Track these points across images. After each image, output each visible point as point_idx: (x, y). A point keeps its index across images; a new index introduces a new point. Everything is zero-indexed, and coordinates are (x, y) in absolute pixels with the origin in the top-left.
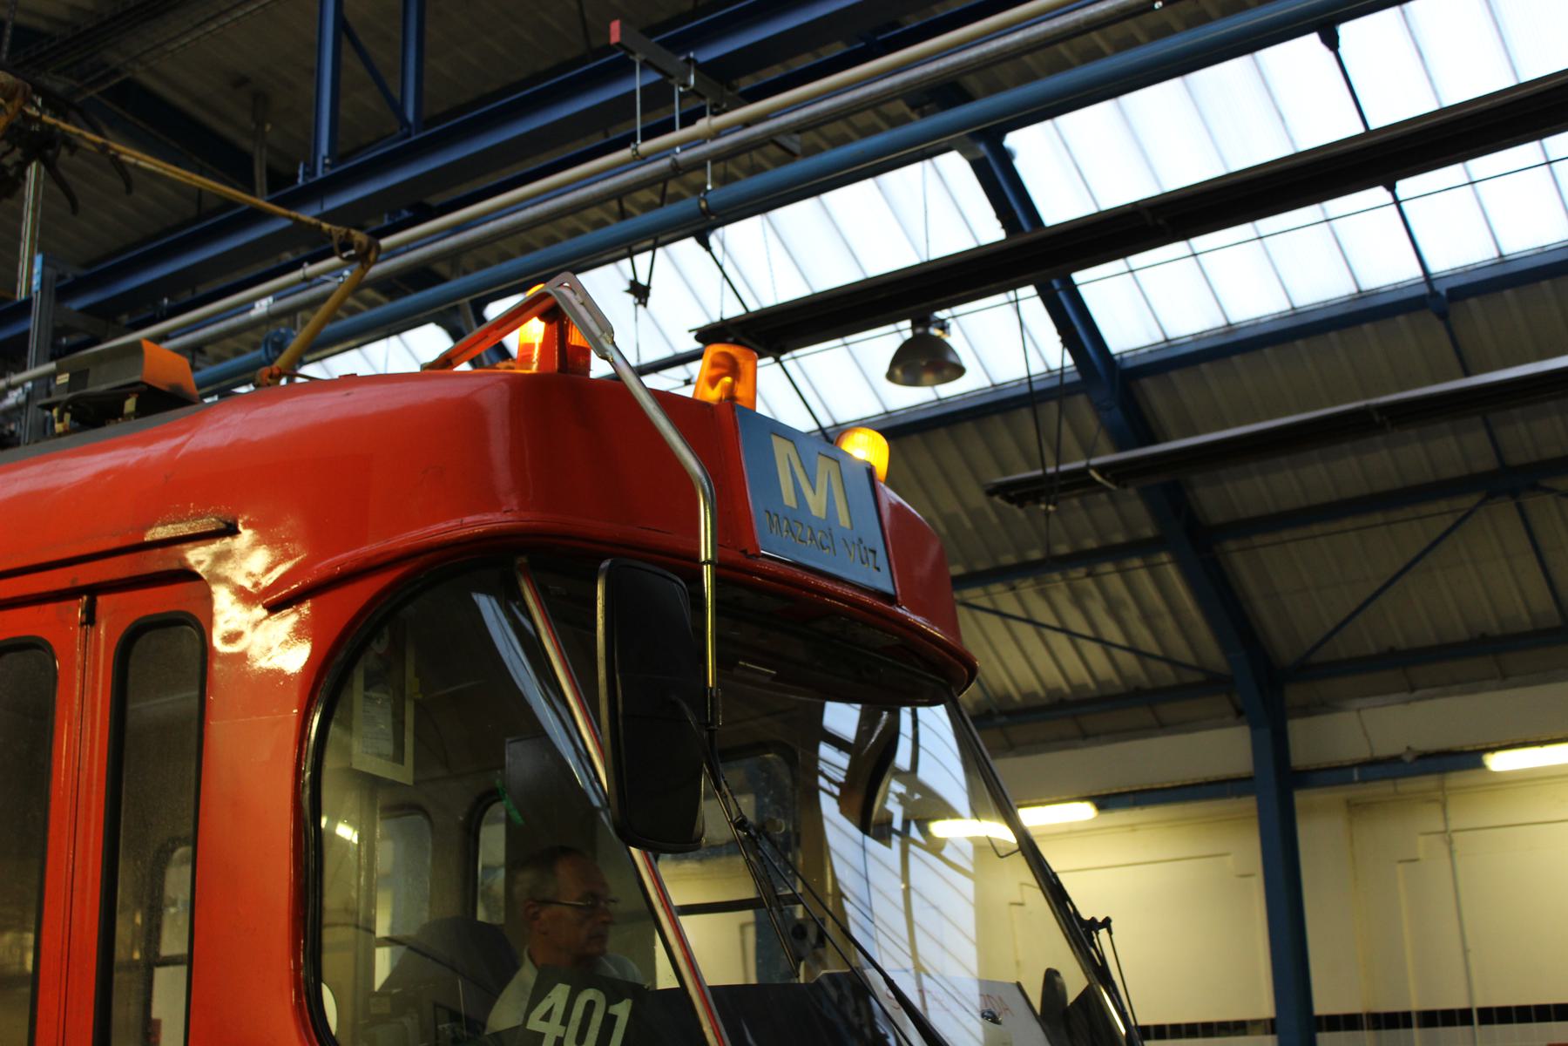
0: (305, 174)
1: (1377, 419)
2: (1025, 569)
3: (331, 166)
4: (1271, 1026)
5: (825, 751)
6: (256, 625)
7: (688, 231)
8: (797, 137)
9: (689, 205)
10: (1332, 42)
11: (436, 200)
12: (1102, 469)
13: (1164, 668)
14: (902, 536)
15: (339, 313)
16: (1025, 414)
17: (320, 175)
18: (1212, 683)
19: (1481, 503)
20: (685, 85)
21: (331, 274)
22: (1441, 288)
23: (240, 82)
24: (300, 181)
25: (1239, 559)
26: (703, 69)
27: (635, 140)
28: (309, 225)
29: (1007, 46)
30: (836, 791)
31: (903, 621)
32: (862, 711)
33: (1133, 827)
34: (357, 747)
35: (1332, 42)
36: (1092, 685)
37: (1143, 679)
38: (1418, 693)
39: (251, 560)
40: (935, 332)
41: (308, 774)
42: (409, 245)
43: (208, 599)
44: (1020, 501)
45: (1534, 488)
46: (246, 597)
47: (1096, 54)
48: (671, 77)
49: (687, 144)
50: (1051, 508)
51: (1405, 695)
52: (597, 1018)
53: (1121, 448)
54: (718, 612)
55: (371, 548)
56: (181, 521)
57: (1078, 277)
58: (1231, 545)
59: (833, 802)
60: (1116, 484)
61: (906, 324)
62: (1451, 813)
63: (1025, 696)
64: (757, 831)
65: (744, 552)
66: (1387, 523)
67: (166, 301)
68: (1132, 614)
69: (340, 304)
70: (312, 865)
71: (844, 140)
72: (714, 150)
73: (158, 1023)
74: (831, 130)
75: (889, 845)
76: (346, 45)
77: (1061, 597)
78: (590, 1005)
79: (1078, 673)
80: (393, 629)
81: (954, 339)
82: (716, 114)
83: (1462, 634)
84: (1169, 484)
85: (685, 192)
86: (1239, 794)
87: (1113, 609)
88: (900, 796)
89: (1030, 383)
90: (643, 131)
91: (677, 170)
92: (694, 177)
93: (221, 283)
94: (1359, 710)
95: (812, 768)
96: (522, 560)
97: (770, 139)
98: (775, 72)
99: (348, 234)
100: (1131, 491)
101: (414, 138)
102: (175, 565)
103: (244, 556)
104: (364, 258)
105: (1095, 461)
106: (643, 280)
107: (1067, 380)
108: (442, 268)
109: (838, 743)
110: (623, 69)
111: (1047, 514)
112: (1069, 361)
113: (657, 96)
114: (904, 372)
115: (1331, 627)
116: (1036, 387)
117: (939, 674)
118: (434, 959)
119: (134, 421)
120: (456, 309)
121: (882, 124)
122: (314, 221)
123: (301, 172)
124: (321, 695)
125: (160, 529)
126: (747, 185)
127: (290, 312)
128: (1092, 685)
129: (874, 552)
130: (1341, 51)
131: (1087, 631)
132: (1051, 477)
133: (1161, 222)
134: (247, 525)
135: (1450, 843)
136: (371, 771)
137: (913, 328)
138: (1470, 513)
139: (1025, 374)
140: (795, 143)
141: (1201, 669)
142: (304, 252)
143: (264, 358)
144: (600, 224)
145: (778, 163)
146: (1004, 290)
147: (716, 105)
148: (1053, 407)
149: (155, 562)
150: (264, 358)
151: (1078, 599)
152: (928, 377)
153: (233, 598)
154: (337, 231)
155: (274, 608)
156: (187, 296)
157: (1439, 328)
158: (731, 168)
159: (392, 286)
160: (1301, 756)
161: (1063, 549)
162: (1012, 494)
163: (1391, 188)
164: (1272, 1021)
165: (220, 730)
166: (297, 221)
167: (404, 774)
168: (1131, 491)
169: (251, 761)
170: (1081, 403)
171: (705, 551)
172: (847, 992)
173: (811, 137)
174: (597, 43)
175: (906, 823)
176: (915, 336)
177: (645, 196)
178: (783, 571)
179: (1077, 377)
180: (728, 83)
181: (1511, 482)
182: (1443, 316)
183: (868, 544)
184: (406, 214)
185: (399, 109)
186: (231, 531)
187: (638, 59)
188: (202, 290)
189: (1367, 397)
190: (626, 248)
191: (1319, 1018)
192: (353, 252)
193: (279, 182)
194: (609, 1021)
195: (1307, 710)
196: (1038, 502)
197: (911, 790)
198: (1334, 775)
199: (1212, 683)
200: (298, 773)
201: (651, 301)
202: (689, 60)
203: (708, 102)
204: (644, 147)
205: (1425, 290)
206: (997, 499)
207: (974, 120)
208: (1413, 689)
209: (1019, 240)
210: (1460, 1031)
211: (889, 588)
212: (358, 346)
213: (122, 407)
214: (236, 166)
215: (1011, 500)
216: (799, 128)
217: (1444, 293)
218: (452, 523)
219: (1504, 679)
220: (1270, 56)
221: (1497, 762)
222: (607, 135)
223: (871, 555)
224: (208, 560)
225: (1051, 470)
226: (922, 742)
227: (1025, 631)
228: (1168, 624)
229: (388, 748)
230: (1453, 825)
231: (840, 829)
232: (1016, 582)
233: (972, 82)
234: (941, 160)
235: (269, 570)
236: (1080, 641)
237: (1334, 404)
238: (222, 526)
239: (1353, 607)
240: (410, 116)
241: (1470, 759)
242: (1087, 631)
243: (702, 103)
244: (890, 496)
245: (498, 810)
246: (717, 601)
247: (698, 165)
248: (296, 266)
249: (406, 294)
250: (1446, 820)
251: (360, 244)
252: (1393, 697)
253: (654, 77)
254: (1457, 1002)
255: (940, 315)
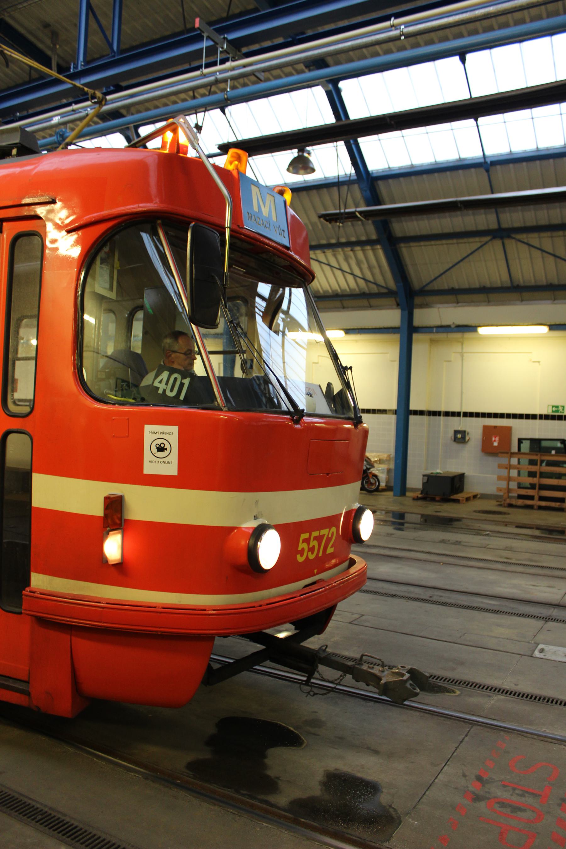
0: (74, 68)
1: (459, 205)
2: (329, 246)
3: (84, 66)
4: (395, 412)
5: (258, 300)
6: (63, 237)
7: (217, 106)
8: (263, 74)
9: (219, 96)
10: (463, 60)
11: (124, 84)
12: (360, 213)
13: (374, 286)
14: (294, 227)
15: (91, 123)
16: (335, 189)
17: (79, 69)
18: (390, 293)
19: (491, 240)
20: (222, 48)
21: (87, 108)
22: (488, 161)
23: (46, 26)
24: (72, 70)
25: (405, 250)
26: (230, 42)
27: (202, 68)
28: (79, 88)
29: (344, 47)
30: (261, 314)
31: (291, 257)
32: (272, 288)
33: (357, 341)
34: (97, 286)
35: (463, 60)
36: (348, 290)
37: (367, 290)
38: (460, 304)
39: (61, 213)
40: (306, 155)
41: (80, 292)
42: (116, 100)
43: (45, 226)
44: (330, 221)
45: (509, 237)
46: (59, 227)
47: (377, 54)
48: (217, 44)
49: (221, 72)
50: (341, 225)
51: (455, 305)
52: (178, 383)
53: (368, 205)
54: (230, 248)
55: (105, 213)
56: (35, 197)
57: (360, 140)
58: (402, 245)
59: (260, 318)
60: (365, 218)
61: (296, 151)
62: (464, 346)
63: (324, 292)
64: (237, 324)
65: (238, 226)
66: (458, 243)
67: (18, 114)
68: (365, 266)
69: (91, 120)
70: (80, 325)
71: (279, 77)
72: (232, 75)
73: (17, 380)
74: (275, 72)
75: (278, 335)
76: (91, 15)
77: (341, 257)
78: (176, 379)
79: (344, 285)
80: (113, 242)
81: (312, 158)
82: (233, 61)
83: (477, 286)
84: (384, 220)
85: (217, 91)
86: (395, 333)
87: (359, 263)
88: (283, 319)
89: (338, 178)
90: (205, 64)
91: (217, 82)
92: (222, 86)
93: (38, 109)
94: (439, 308)
95: (253, 305)
96: (159, 222)
97: (253, 73)
98: (256, 47)
99: (94, 93)
100: (370, 222)
101: (116, 58)
102: (33, 213)
103: (58, 212)
104: (100, 103)
105: (359, 209)
106: (200, 124)
107: (352, 178)
108: (123, 112)
109: (263, 298)
110: (199, 38)
111: (339, 227)
112: (353, 171)
113: (211, 51)
114: (293, 168)
115: (433, 278)
116: (340, 180)
117: (302, 277)
118: (118, 362)
119: (16, 158)
120: (128, 128)
121: (294, 72)
122: (81, 86)
123: (72, 67)
124: (85, 264)
125: (27, 199)
126: (242, 91)
127: (65, 124)
128: (348, 290)
129: (284, 231)
130: (466, 65)
131: (348, 271)
132: (342, 214)
133: (393, 122)
134: (60, 200)
135: (462, 356)
136: (102, 294)
137: (298, 152)
138: (486, 243)
139: (337, 175)
140: (262, 76)
141: (387, 288)
142: (71, 100)
143: (56, 140)
144: (184, 100)
145: (254, 83)
146: (333, 142)
147: (233, 57)
148: (345, 188)
149: (25, 212)
150: (56, 140)
151: (347, 259)
152: (302, 171)
153: (53, 227)
154: (90, 91)
155: (69, 232)
156: (25, 113)
157: (486, 174)
158: (236, 84)
159: (104, 117)
160: (417, 322)
161: (343, 240)
162: (327, 218)
163: (476, 120)
164: (396, 411)
165: (48, 275)
166: (75, 86)
167: (112, 295)
168: (370, 222)
169: (59, 287)
170: (356, 187)
171: (227, 223)
172: (262, 382)
173: (267, 75)
174: (189, 26)
175: (284, 328)
176: (299, 156)
177: (202, 91)
178: (252, 235)
179: (355, 178)
180: (239, 48)
181: (501, 234)
182: (487, 171)
183: (282, 228)
184: (112, 88)
185: (111, 45)
186: (54, 202)
187: (205, 35)
188: (31, 111)
189: (457, 197)
190: (195, 110)
191: (411, 411)
192: (96, 100)
193: (61, 70)
194: (182, 385)
195: (421, 306)
196: (336, 222)
197: (286, 318)
198: (427, 329)
199: (390, 293)
200: (76, 292)
201: (202, 131)
202: (224, 38)
203: (230, 56)
204: (206, 71)
205: (482, 160)
206: (322, 219)
207: (328, 74)
208: (458, 303)
209: (340, 123)
210: (456, 419)
211: (288, 245)
212: (90, 139)
213: (11, 152)
214: (46, 61)
215: (327, 220)
216: (264, 70)
217: (489, 162)
218: (135, 206)
219: (489, 302)
220: (440, 63)
221: (482, 331)
222: (190, 65)
223: (282, 232)
224: (45, 212)
225: (342, 211)
226: (292, 300)
227: (327, 268)
228: (377, 271)
229: (107, 286)
230: (464, 350)
231: (263, 328)
232: (326, 250)
233: (329, 60)
234: (314, 89)
235: (67, 217)
236: (346, 274)
237: (557, 185)
238: (51, 200)
239: (442, 272)
240: (115, 48)
241: (472, 328)
242: (348, 271)
243: (228, 56)
244: (291, 211)
245: (140, 315)
246: (230, 244)
247: (225, 81)
248: (69, 105)
249: (109, 120)
250: (462, 348)
251: (99, 98)
252: (451, 305)
253: (211, 43)
254: (457, 409)
255: (308, 148)
